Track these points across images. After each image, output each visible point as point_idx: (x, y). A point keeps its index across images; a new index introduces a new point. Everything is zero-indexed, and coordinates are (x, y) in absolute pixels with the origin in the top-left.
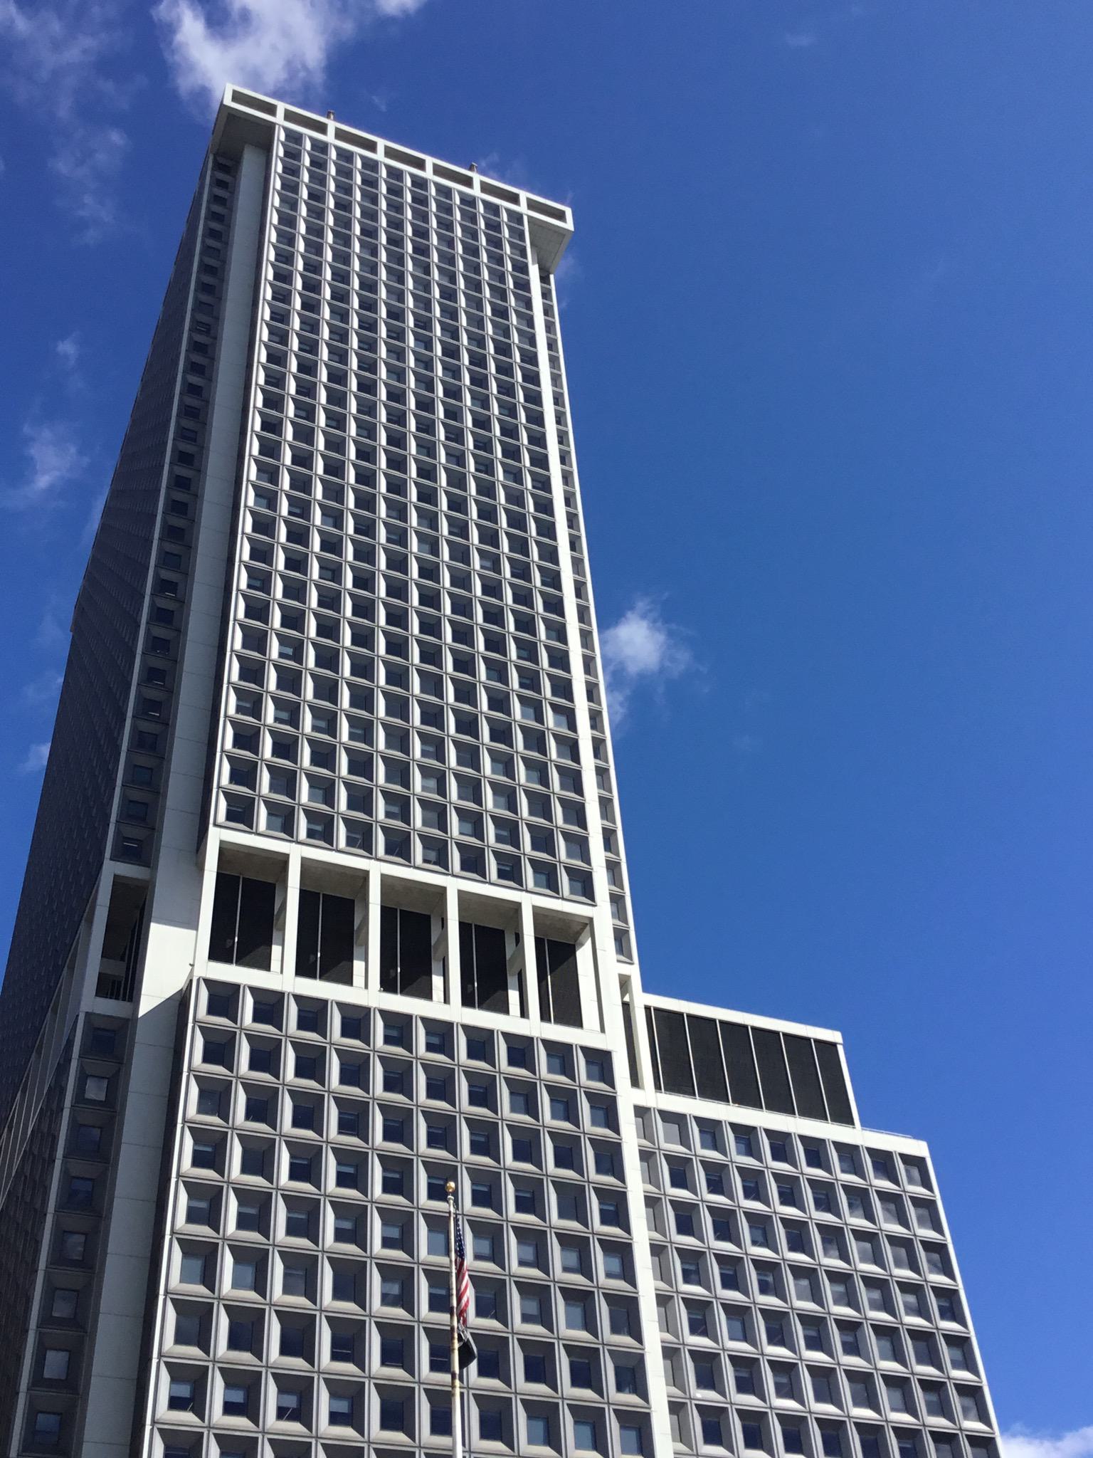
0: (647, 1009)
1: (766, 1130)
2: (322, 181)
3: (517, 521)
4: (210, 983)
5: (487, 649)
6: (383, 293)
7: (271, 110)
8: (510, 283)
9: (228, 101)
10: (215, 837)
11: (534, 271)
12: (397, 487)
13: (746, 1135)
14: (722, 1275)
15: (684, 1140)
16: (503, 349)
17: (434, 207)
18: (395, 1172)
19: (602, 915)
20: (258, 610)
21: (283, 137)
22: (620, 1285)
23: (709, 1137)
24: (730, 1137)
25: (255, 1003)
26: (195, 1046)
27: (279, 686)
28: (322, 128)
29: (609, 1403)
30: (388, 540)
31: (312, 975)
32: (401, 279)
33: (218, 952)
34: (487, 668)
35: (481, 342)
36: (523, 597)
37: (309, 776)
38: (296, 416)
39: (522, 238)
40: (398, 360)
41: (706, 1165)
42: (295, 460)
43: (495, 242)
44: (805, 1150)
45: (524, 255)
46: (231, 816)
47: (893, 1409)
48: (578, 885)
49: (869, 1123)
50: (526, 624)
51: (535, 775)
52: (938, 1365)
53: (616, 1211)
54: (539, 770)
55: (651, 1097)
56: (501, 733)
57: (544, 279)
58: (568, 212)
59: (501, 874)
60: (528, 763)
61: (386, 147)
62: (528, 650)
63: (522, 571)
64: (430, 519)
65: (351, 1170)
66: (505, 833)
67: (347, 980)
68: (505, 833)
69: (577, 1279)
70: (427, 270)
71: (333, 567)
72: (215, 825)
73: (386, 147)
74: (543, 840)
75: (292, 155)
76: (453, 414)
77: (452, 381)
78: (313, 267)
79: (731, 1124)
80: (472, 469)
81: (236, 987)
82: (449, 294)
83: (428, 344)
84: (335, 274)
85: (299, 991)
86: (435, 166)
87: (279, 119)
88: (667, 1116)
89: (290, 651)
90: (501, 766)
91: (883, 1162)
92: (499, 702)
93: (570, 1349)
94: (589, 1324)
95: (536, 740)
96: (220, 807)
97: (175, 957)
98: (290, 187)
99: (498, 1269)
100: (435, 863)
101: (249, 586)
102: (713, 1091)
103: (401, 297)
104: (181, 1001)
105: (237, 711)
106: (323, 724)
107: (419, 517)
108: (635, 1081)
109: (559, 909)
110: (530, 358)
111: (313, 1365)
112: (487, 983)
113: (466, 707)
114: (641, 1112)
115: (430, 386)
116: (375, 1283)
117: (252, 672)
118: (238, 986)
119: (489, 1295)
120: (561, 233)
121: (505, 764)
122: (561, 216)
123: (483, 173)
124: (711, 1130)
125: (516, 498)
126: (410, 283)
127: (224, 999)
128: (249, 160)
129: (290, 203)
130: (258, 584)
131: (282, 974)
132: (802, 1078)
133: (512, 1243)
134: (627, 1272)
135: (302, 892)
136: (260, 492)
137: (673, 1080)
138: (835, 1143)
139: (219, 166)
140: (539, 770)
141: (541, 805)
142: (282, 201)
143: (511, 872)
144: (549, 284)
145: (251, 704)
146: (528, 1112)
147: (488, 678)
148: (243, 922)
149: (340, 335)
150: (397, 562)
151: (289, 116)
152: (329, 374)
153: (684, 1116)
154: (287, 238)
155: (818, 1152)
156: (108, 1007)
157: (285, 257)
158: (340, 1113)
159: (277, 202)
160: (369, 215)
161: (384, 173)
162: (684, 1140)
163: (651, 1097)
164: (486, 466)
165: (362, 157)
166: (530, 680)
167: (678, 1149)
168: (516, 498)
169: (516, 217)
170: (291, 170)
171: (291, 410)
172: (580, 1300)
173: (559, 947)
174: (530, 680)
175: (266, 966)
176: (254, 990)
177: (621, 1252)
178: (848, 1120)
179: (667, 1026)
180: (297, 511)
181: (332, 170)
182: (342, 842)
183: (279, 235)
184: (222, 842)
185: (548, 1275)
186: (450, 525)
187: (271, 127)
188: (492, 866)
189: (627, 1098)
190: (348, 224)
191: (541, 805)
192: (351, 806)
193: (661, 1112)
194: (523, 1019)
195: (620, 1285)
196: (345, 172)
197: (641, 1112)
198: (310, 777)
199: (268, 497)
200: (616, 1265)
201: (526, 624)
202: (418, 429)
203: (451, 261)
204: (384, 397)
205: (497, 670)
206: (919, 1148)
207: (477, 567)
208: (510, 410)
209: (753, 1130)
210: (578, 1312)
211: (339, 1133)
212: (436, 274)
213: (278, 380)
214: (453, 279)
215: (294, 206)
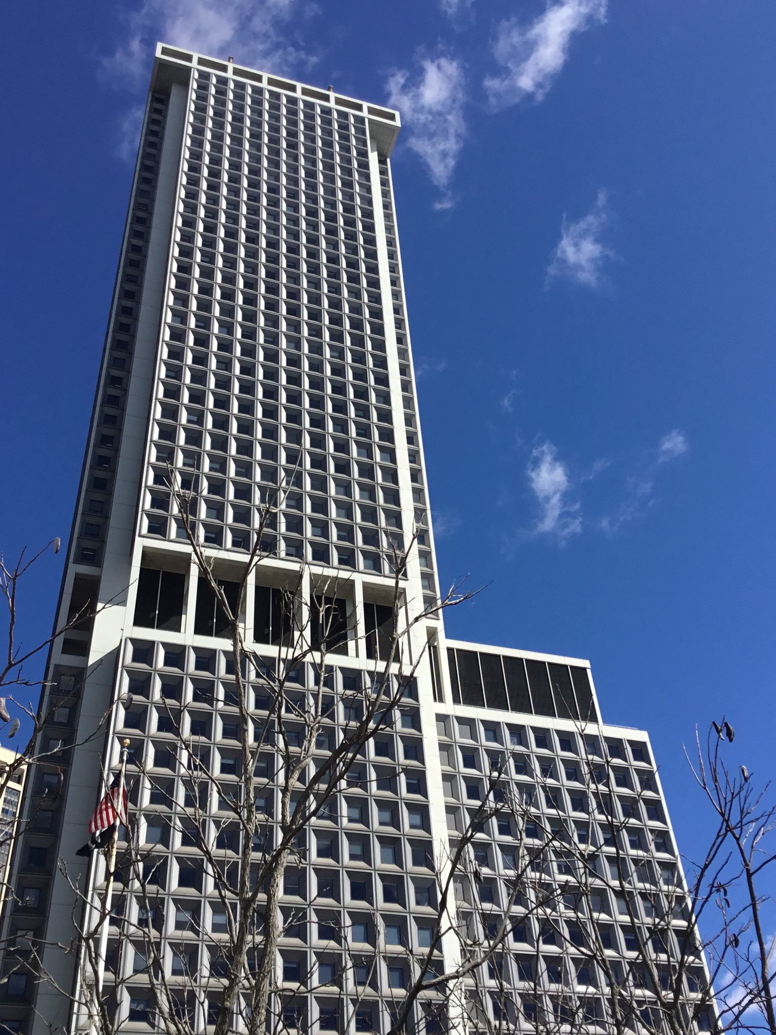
0: (450, 650)
1: (532, 727)
2: (242, 108)
3: (357, 325)
4: (133, 641)
5: (379, 420)
6: (265, 176)
7: (189, 58)
8: (355, 164)
9: (158, 54)
10: (140, 544)
11: (373, 158)
12: (272, 305)
13: (518, 731)
14: (499, 826)
15: (474, 736)
16: (349, 209)
17: (302, 116)
18: (229, 759)
19: (414, 587)
20: (172, 392)
21: (196, 76)
22: (420, 833)
23: (491, 734)
24: (506, 733)
25: (166, 653)
26: (124, 684)
27: (263, 457)
28: (326, 98)
29: (410, 913)
30: (265, 341)
31: (209, 634)
32: (277, 165)
33: (140, 620)
34: (334, 424)
35: (333, 205)
36: (360, 375)
37: (311, 519)
38: (202, 261)
39: (364, 133)
40: (314, 230)
41: (489, 752)
42: (201, 291)
43: (345, 138)
44: (560, 740)
45: (365, 144)
46: (151, 530)
47: (621, 913)
48: (371, 563)
49: (609, 720)
50: (361, 393)
51: (366, 494)
52: (654, 883)
53: (418, 783)
54: (369, 491)
55: (449, 707)
56: (343, 467)
57: (382, 161)
58: (397, 115)
59: (341, 561)
60: (362, 487)
61: (369, 108)
62: (363, 411)
63: (359, 358)
64: (295, 326)
65: (231, 762)
66: (344, 534)
67: (344, 651)
68: (344, 534)
69: (390, 830)
70: (296, 159)
71: (227, 361)
72: (140, 536)
73: (369, 108)
74: (371, 537)
75: (203, 87)
76: (313, 254)
77: (292, 227)
78: (216, 161)
79: (507, 724)
80: (366, 300)
81: (152, 643)
82: (311, 174)
83: (296, 209)
84: (307, 185)
85: (196, 645)
86: (336, 99)
87: (194, 64)
88: (461, 720)
89: (195, 419)
90: (342, 489)
91: (616, 747)
92: (342, 446)
93: (383, 877)
94: (398, 860)
95: (367, 471)
96: (144, 524)
97: (113, 627)
98: (201, 108)
99: (333, 825)
100: (296, 556)
101: (167, 376)
102: (498, 703)
103: (277, 178)
104: (115, 654)
105: (236, 475)
106: (217, 466)
107: (287, 325)
108: (438, 696)
109: (227, 558)
110: (368, 214)
111: (201, 892)
112: (333, 637)
113: (318, 450)
114: (441, 718)
115: (297, 236)
116: (345, 847)
117: (162, 477)
118: (215, 650)
119: (327, 843)
120: (393, 129)
121: (345, 487)
122: (392, 117)
123: (335, 91)
124: (493, 729)
125: (356, 309)
126: (284, 168)
127: (144, 651)
128: (175, 92)
129: (200, 119)
130: (173, 374)
131: (187, 635)
132: (558, 691)
133: (405, 814)
134: (425, 824)
135: (257, 587)
136: (175, 313)
137: (468, 694)
138: (628, 741)
139: (155, 99)
140: (369, 491)
141: (370, 514)
142: (195, 118)
143: (347, 560)
144: (386, 164)
145: (167, 454)
146: (413, 727)
147: (334, 431)
148: (160, 598)
149: (294, 221)
150: (272, 356)
151: (201, 62)
152: (267, 243)
153: (473, 720)
154: (198, 143)
155: (569, 741)
156: (70, 660)
157: (196, 156)
158: (224, 724)
159: (191, 119)
160: (256, 123)
161: (302, 106)
162: (474, 736)
163: (449, 707)
164: (336, 289)
165: (286, 96)
166: (364, 431)
167: (469, 742)
168: (356, 309)
169: (360, 120)
170: (202, 98)
171: (198, 257)
172: (392, 844)
173: (383, 611)
174: (364, 431)
175: (178, 630)
176: (164, 645)
177: (421, 812)
178: (594, 719)
179: (464, 663)
180: (202, 325)
181: (231, 96)
182: (335, 561)
183: (192, 141)
184: (144, 547)
185: (368, 827)
186: (309, 330)
187: (188, 70)
188: (335, 556)
189: (428, 708)
190: (241, 131)
191: (370, 514)
192: (288, 529)
193: (457, 718)
194: (356, 657)
195: (420, 833)
196: (275, 107)
197: (441, 718)
198: (312, 520)
199: (181, 316)
200: (417, 820)
201: (361, 393)
202: (328, 276)
203: (313, 151)
204: (344, 266)
205: (341, 425)
206: (642, 736)
207: (328, 356)
208: (353, 250)
209: (522, 727)
210: (390, 852)
211: (223, 738)
212: (302, 161)
213: (190, 237)
214: (314, 163)
215: (203, 121)
